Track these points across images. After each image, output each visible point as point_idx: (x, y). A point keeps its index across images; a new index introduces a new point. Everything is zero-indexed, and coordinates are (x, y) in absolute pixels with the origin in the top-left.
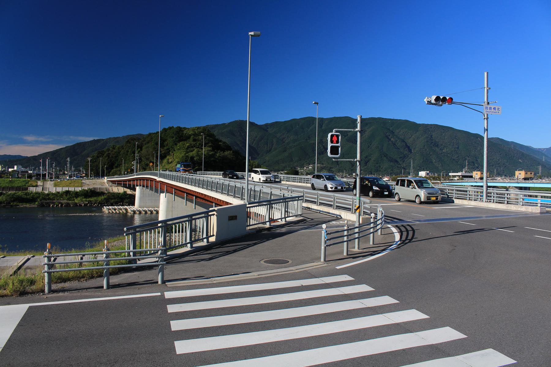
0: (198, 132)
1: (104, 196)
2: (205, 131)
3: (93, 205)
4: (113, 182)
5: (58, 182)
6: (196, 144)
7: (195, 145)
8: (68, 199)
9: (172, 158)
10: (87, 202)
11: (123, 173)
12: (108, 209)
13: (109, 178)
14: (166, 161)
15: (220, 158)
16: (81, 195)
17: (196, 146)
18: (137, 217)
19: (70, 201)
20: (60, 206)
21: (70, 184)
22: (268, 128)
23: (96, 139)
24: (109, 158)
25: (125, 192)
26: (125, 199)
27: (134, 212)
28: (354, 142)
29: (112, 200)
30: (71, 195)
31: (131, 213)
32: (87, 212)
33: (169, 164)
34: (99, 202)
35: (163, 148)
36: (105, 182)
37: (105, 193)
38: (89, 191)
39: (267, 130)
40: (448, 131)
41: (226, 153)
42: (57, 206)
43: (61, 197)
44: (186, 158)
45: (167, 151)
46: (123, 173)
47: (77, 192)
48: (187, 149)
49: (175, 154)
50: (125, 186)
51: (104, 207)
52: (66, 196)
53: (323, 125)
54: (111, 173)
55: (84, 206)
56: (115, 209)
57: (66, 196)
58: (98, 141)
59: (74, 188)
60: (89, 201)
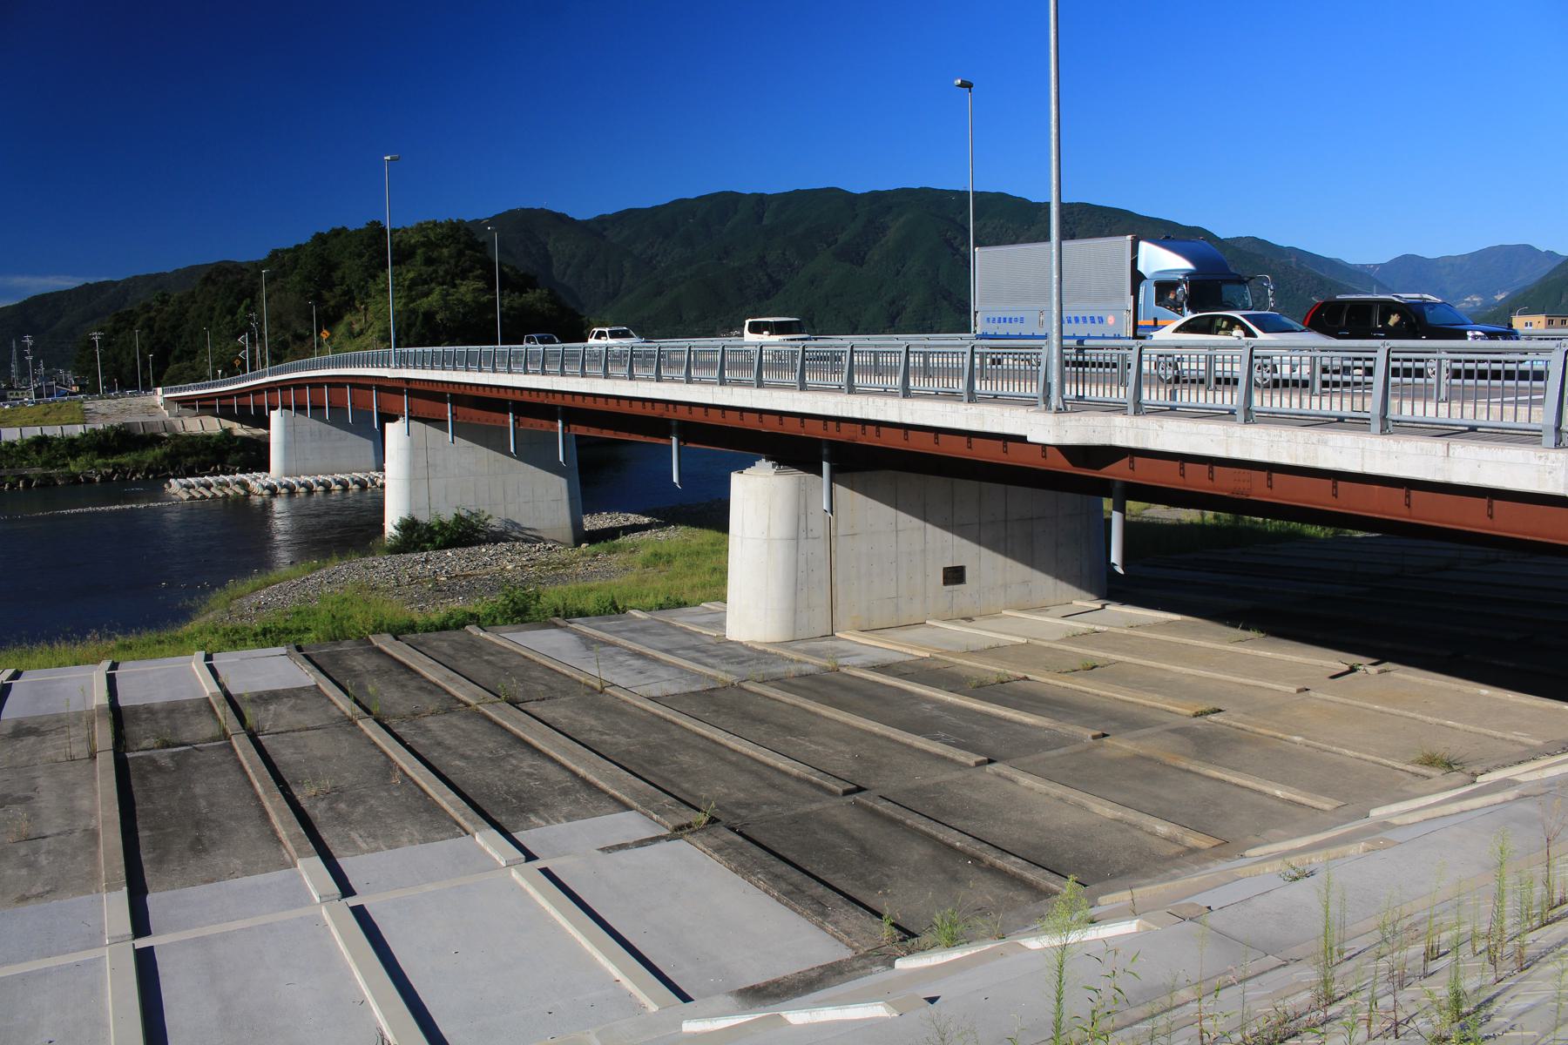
0: (438, 235)
1: (160, 448)
2: (458, 231)
3: (131, 477)
4: (186, 403)
5: (3, 412)
6: (436, 271)
7: (434, 275)
8: (45, 464)
9: (360, 320)
10: (111, 470)
11: (209, 373)
12: (185, 486)
13: (171, 391)
14: (343, 330)
15: (512, 312)
16: (89, 449)
17: (437, 278)
18: (279, 505)
19: (53, 468)
20: (21, 485)
21: (45, 415)
22: (605, 229)
23: (91, 283)
24: (152, 331)
25: (228, 432)
26: (228, 454)
27: (273, 491)
28: (855, 261)
29: (189, 459)
30: (53, 452)
31: (261, 495)
32: (122, 502)
33: (354, 337)
34: (148, 468)
35: (332, 291)
36: (159, 403)
37: (164, 438)
38: (112, 435)
39: (605, 233)
40: (1119, 221)
41: (530, 297)
42: (12, 486)
43: (21, 457)
44: (409, 318)
45: (343, 298)
46: (209, 373)
47: (72, 441)
48: (410, 288)
49: (371, 308)
50: (226, 413)
51: (172, 481)
52: (37, 454)
53: (764, 213)
54: (165, 377)
55: (101, 481)
56: (208, 486)
57: (39, 453)
58: (101, 287)
59: (59, 427)
60: (114, 465)
